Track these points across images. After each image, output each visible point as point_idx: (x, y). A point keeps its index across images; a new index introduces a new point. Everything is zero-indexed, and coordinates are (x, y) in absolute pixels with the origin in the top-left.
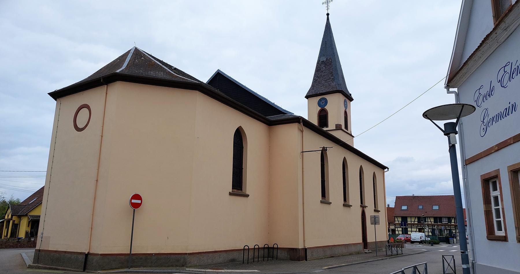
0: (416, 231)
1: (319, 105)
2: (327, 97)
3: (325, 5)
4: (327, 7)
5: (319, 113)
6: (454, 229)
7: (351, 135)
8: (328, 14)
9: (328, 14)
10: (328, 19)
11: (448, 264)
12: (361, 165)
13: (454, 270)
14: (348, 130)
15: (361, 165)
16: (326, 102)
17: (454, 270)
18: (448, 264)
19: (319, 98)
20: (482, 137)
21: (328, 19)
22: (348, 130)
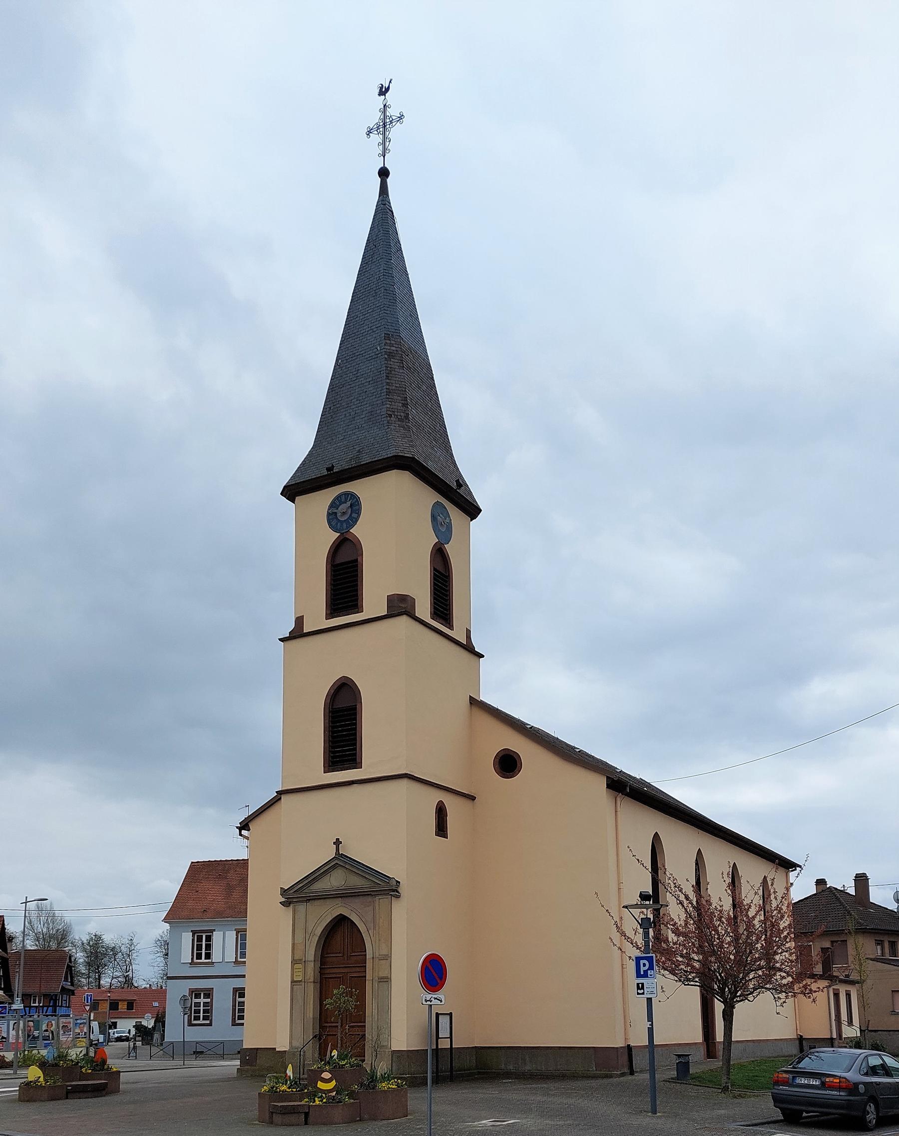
0: (25, 901)
1: (332, 519)
2: (357, 487)
3: (377, 138)
4: (384, 143)
5: (332, 551)
6: (66, 1005)
7: (469, 648)
8: (384, 173)
9: (384, 173)
10: (384, 190)
11: (384, 157)
12: (699, 849)
13: (640, 922)
14: (451, 627)
15: (699, 849)
16: (354, 504)
17: (640, 922)
18: (384, 157)
19: (326, 497)
20: (423, 1004)
21: (384, 190)
22: (451, 627)
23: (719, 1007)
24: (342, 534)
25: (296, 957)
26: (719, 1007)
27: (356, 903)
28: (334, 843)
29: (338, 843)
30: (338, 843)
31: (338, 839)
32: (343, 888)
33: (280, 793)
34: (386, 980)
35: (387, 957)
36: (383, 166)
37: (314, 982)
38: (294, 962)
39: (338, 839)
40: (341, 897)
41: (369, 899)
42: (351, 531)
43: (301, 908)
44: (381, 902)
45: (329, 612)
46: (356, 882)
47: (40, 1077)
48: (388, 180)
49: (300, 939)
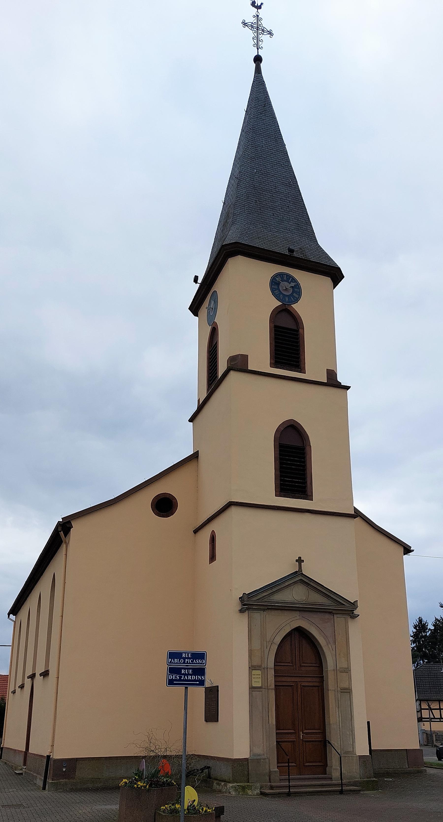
8: (258, 60)
9: (258, 60)
10: (258, 71)
21: (258, 71)
23: (423, 720)
24: (284, 304)
25: (255, 664)
26: (423, 720)
27: (316, 618)
28: (297, 561)
29: (300, 561)
30: (300, 561)
31: (300, 558)
32: (304, 602)
33: (230, 504)
34: (348, 691)
35: (347, 670)
36: (257, 54)
37: (328, 690)
38: (252, 668)
39: (300, 558)
40: (300, 611)
41: (327, 616)
42: (292, 305)
43: (257, 616)
44: (339, 620)
45: (273, 362)
46: (316, 598)
47: (194, 800)
48: (262, 65)
49: (257, 645)
